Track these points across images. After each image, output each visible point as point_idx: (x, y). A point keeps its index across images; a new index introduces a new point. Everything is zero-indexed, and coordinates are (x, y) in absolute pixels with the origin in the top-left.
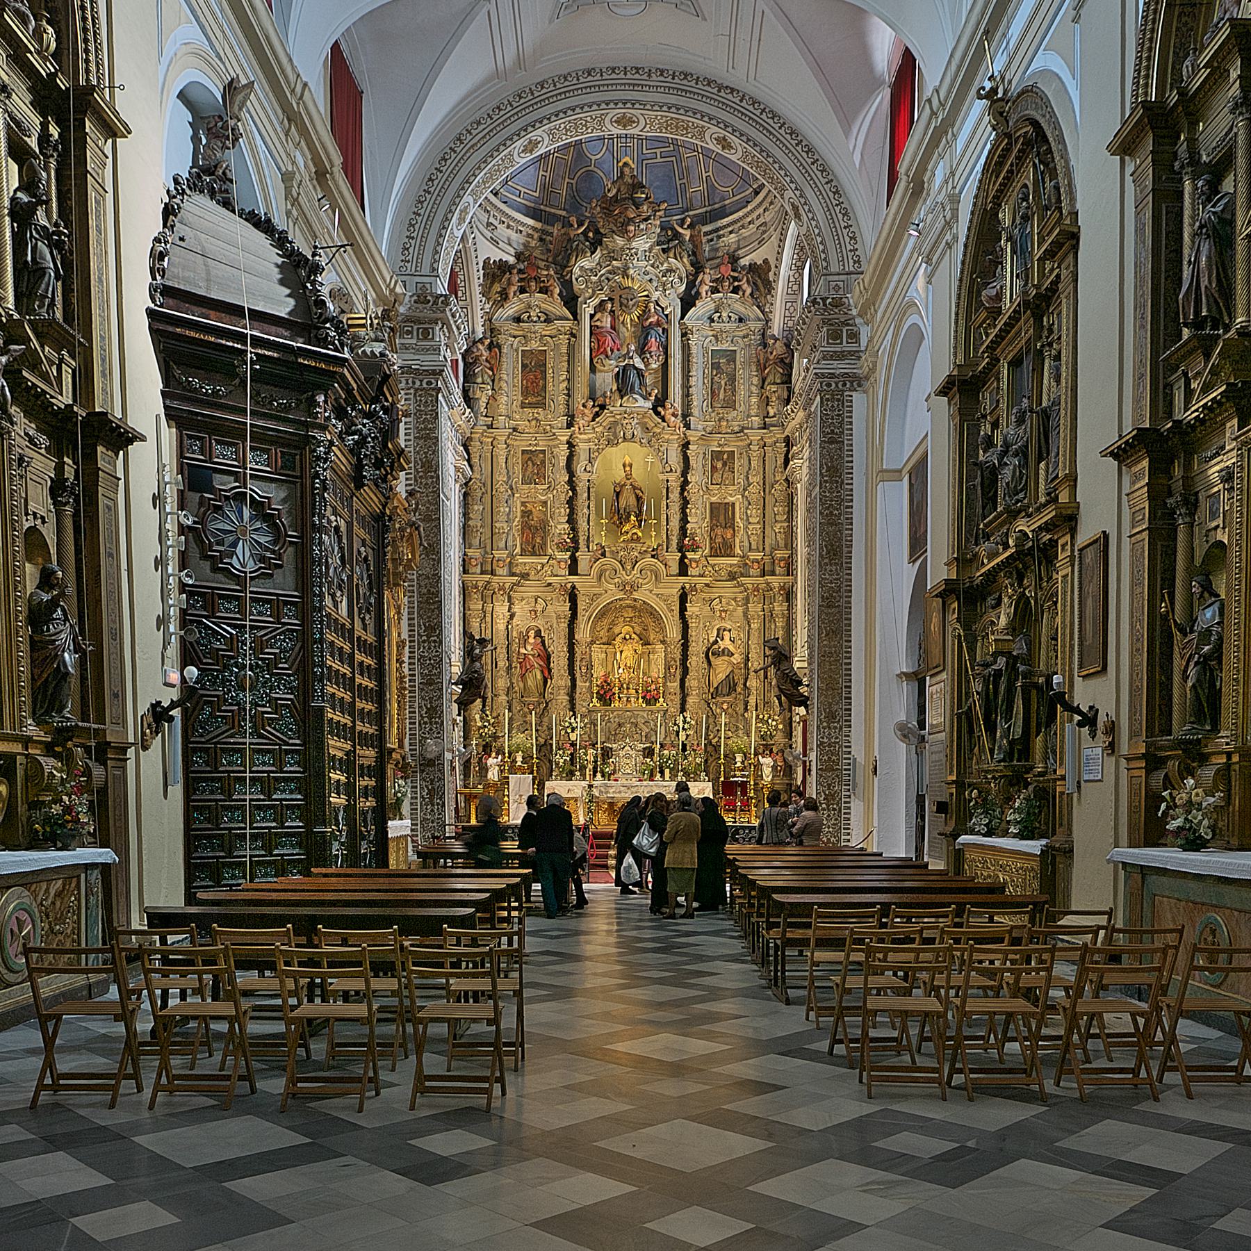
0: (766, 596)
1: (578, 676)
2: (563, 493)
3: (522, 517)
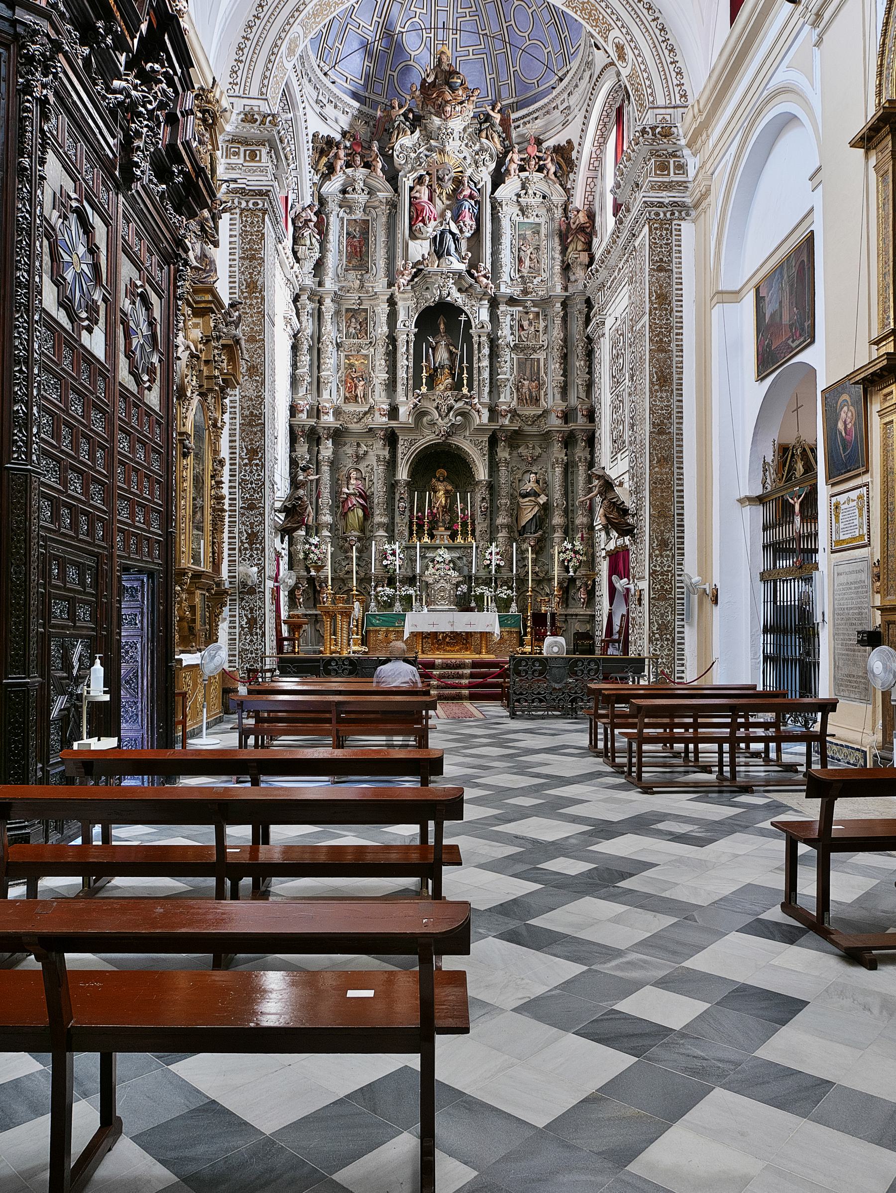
3: (346, 368)
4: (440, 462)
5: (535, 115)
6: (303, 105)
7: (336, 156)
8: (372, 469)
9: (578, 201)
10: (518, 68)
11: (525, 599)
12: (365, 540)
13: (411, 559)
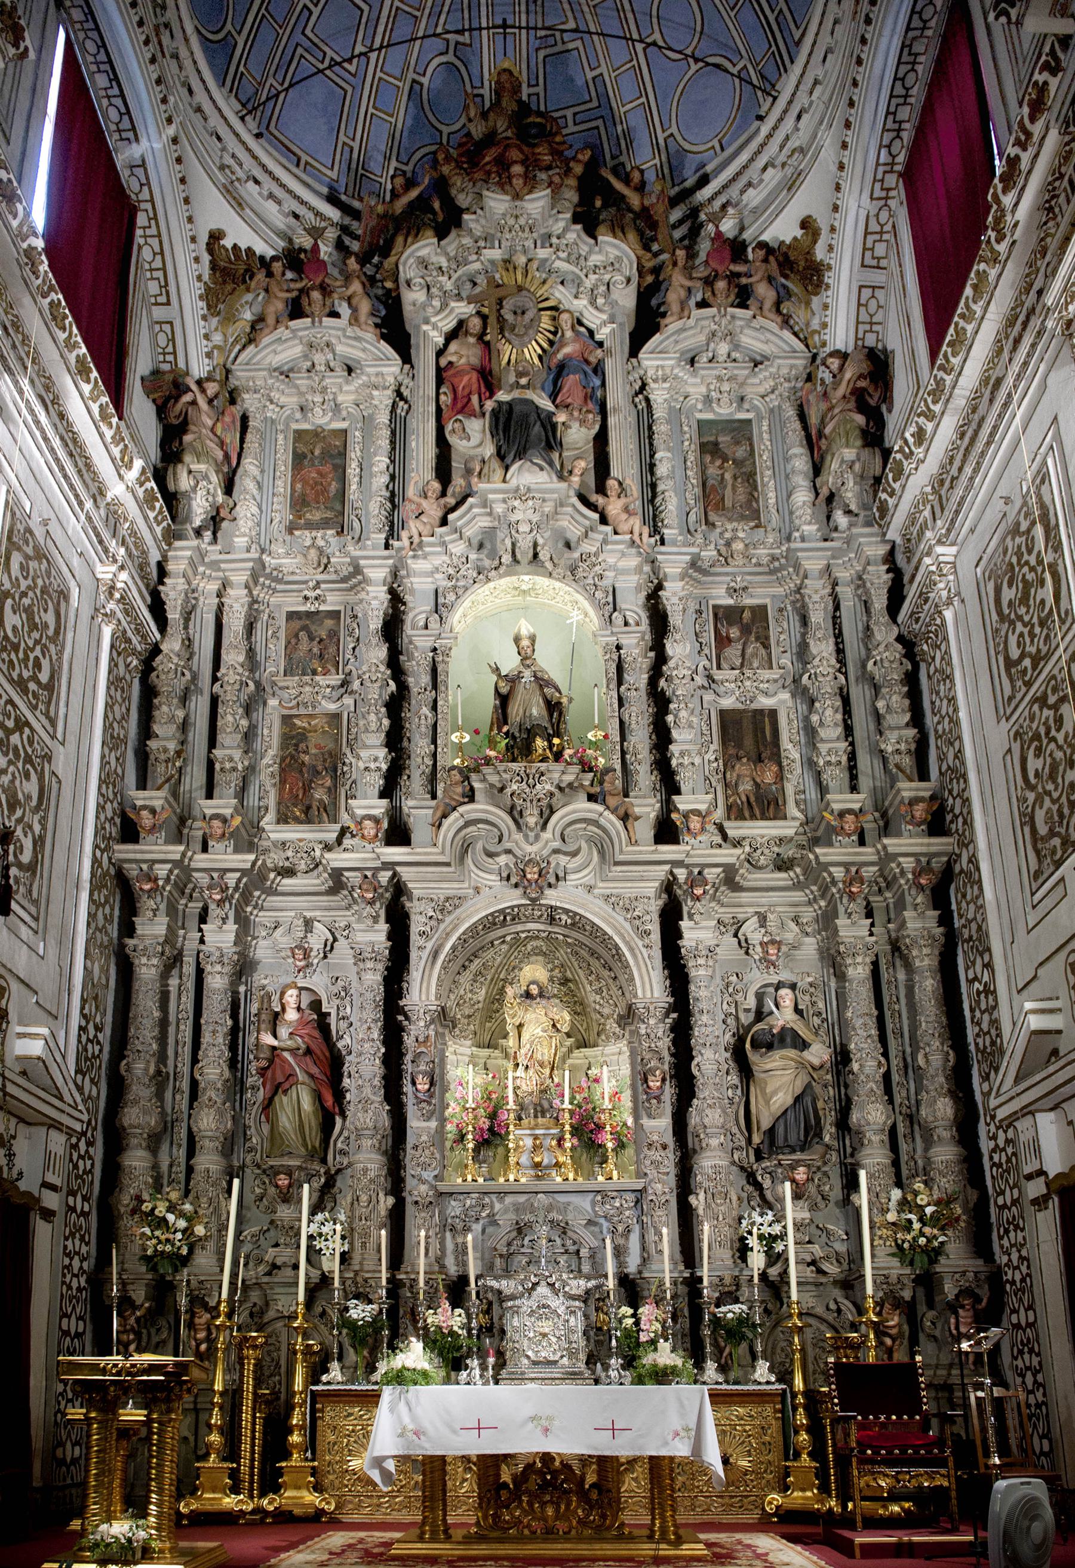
0: (878, 897)
1: (409, 1101)
2: (377, 687)
3: (283, 746)
10: (674, 129)
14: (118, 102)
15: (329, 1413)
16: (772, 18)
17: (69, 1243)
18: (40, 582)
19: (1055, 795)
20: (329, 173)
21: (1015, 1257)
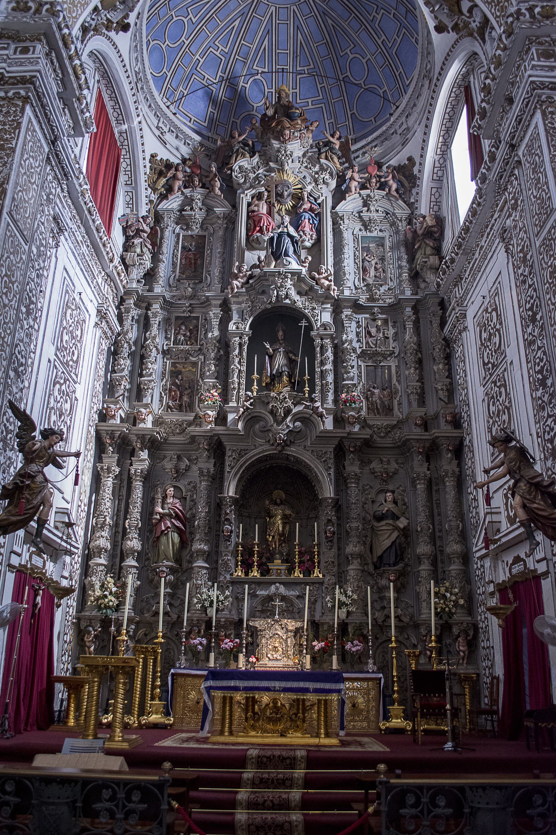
4: (276, 480)
5: (374, 144)
6: (139, 119)
7: (175, 177)
8: (195, 487)
9: (424, 208)
10: (355, 111)
11: (386, 652)
12: (182, 570)
13: (237, 598)
14: (118, 111)
15: (180, 680)
16: (397, 74)
17: (69, 602)
18: (76, 319)
19: (499, 423)
20: (204, 124)
21: (483, 617)
